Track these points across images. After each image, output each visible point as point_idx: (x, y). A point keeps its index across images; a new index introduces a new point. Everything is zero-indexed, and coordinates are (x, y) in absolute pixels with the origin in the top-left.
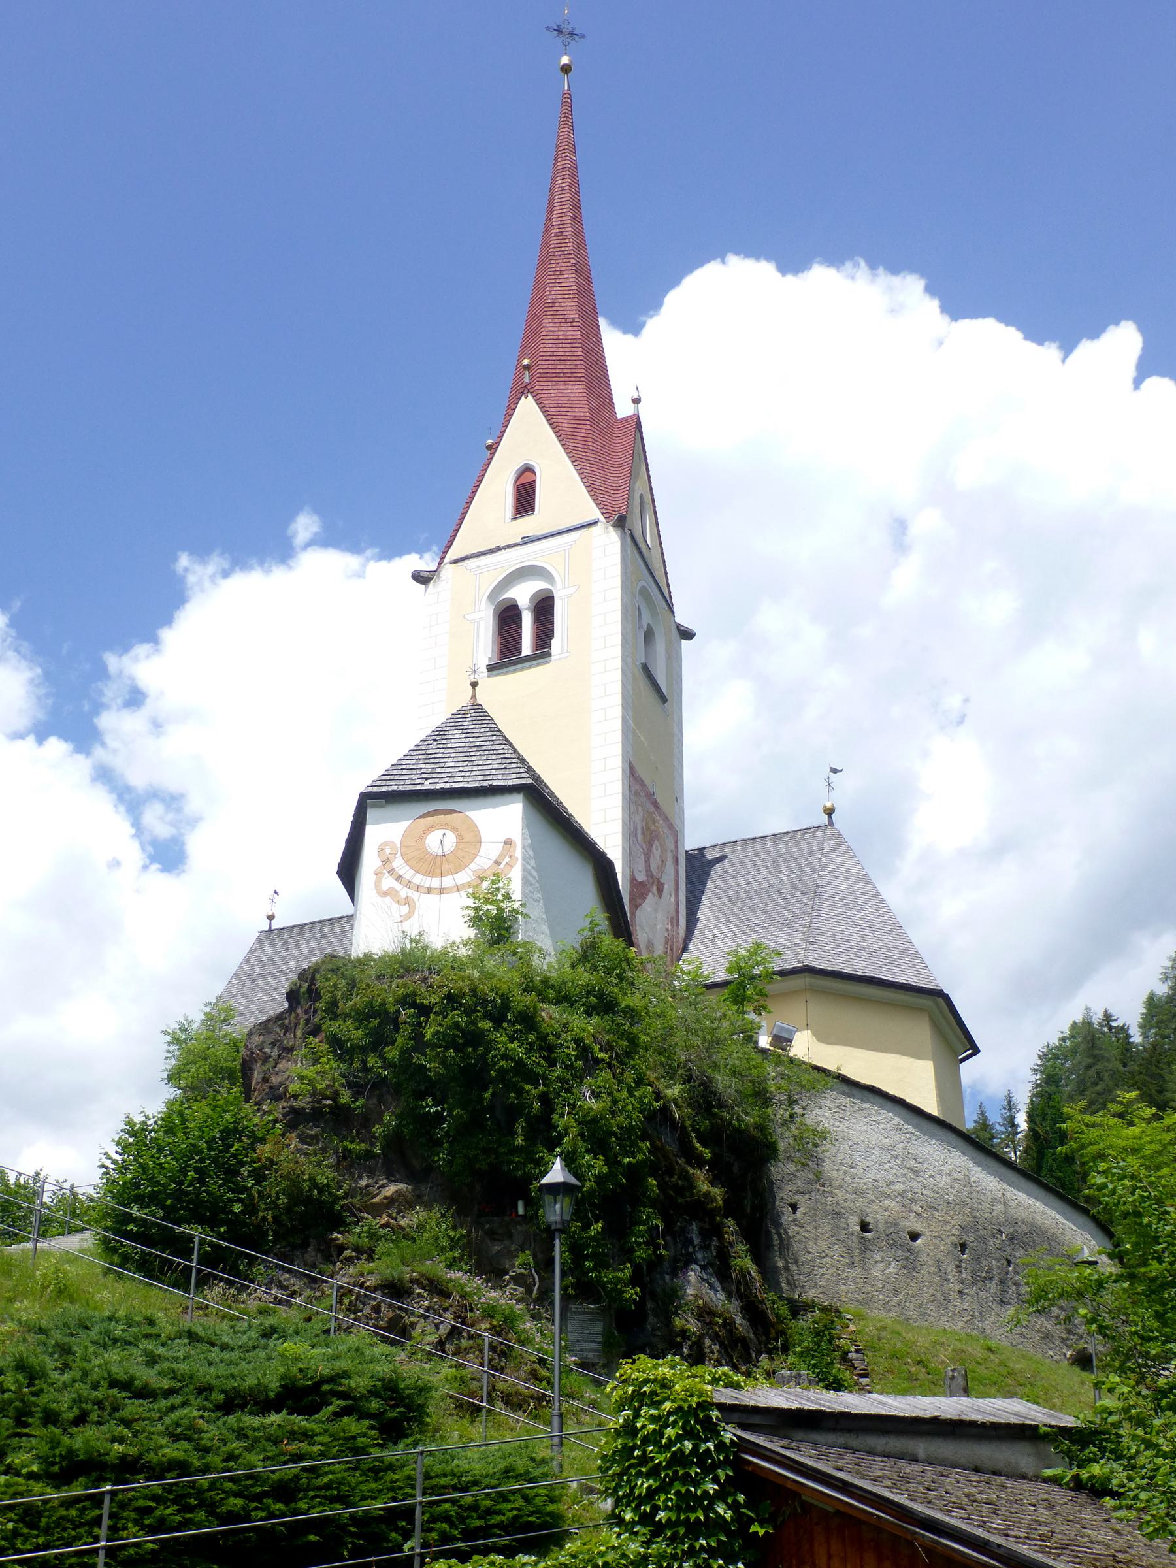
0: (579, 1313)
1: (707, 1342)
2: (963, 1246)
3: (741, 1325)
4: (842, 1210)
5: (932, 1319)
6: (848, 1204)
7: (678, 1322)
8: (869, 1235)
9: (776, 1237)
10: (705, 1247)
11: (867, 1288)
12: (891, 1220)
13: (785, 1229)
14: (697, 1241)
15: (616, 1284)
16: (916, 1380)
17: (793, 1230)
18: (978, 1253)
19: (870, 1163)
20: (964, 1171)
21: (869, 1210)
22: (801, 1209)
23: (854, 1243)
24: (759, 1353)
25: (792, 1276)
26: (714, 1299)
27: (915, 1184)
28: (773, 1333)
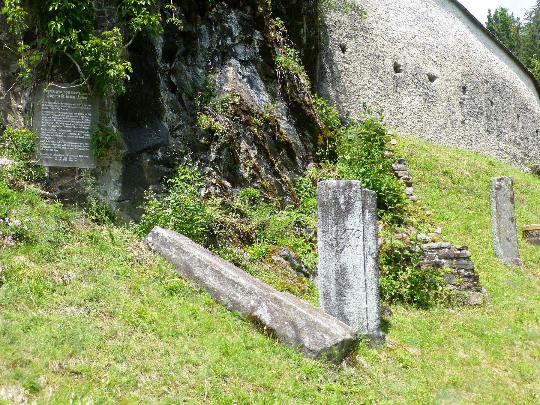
0: (59, 100)
1: (244, 146)
2: (464, 88)
3: (286, 129)
4: (380, 54)
5: (444, 141)
6: (384, 49)
7: (204, 120)
8: (400, 75)
9: (328, 70)
10: (248, 41)
11: (398, 116)
12: (415, 64)
13: (336, 66)
14: (236, 32)
15: (97, 56)
16: (445, 188)
17: (342, 66)
18: (473, 94)
19: (400, 20)
20: (464, 35)
21: (400, 55)
22: (349, 50)
23: (389, 79)
24: (306, 161)
25: (341, 103)
26: (256, 99)
27: (432, 39)
28: (320, 141)
